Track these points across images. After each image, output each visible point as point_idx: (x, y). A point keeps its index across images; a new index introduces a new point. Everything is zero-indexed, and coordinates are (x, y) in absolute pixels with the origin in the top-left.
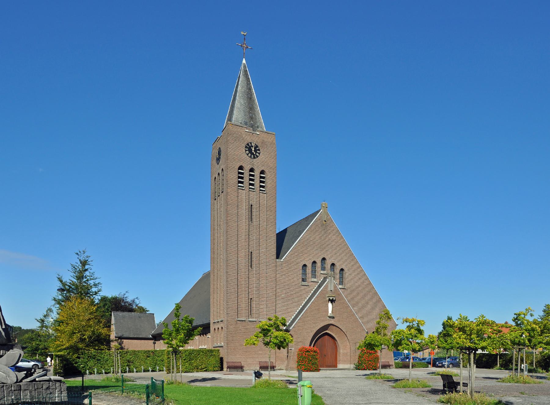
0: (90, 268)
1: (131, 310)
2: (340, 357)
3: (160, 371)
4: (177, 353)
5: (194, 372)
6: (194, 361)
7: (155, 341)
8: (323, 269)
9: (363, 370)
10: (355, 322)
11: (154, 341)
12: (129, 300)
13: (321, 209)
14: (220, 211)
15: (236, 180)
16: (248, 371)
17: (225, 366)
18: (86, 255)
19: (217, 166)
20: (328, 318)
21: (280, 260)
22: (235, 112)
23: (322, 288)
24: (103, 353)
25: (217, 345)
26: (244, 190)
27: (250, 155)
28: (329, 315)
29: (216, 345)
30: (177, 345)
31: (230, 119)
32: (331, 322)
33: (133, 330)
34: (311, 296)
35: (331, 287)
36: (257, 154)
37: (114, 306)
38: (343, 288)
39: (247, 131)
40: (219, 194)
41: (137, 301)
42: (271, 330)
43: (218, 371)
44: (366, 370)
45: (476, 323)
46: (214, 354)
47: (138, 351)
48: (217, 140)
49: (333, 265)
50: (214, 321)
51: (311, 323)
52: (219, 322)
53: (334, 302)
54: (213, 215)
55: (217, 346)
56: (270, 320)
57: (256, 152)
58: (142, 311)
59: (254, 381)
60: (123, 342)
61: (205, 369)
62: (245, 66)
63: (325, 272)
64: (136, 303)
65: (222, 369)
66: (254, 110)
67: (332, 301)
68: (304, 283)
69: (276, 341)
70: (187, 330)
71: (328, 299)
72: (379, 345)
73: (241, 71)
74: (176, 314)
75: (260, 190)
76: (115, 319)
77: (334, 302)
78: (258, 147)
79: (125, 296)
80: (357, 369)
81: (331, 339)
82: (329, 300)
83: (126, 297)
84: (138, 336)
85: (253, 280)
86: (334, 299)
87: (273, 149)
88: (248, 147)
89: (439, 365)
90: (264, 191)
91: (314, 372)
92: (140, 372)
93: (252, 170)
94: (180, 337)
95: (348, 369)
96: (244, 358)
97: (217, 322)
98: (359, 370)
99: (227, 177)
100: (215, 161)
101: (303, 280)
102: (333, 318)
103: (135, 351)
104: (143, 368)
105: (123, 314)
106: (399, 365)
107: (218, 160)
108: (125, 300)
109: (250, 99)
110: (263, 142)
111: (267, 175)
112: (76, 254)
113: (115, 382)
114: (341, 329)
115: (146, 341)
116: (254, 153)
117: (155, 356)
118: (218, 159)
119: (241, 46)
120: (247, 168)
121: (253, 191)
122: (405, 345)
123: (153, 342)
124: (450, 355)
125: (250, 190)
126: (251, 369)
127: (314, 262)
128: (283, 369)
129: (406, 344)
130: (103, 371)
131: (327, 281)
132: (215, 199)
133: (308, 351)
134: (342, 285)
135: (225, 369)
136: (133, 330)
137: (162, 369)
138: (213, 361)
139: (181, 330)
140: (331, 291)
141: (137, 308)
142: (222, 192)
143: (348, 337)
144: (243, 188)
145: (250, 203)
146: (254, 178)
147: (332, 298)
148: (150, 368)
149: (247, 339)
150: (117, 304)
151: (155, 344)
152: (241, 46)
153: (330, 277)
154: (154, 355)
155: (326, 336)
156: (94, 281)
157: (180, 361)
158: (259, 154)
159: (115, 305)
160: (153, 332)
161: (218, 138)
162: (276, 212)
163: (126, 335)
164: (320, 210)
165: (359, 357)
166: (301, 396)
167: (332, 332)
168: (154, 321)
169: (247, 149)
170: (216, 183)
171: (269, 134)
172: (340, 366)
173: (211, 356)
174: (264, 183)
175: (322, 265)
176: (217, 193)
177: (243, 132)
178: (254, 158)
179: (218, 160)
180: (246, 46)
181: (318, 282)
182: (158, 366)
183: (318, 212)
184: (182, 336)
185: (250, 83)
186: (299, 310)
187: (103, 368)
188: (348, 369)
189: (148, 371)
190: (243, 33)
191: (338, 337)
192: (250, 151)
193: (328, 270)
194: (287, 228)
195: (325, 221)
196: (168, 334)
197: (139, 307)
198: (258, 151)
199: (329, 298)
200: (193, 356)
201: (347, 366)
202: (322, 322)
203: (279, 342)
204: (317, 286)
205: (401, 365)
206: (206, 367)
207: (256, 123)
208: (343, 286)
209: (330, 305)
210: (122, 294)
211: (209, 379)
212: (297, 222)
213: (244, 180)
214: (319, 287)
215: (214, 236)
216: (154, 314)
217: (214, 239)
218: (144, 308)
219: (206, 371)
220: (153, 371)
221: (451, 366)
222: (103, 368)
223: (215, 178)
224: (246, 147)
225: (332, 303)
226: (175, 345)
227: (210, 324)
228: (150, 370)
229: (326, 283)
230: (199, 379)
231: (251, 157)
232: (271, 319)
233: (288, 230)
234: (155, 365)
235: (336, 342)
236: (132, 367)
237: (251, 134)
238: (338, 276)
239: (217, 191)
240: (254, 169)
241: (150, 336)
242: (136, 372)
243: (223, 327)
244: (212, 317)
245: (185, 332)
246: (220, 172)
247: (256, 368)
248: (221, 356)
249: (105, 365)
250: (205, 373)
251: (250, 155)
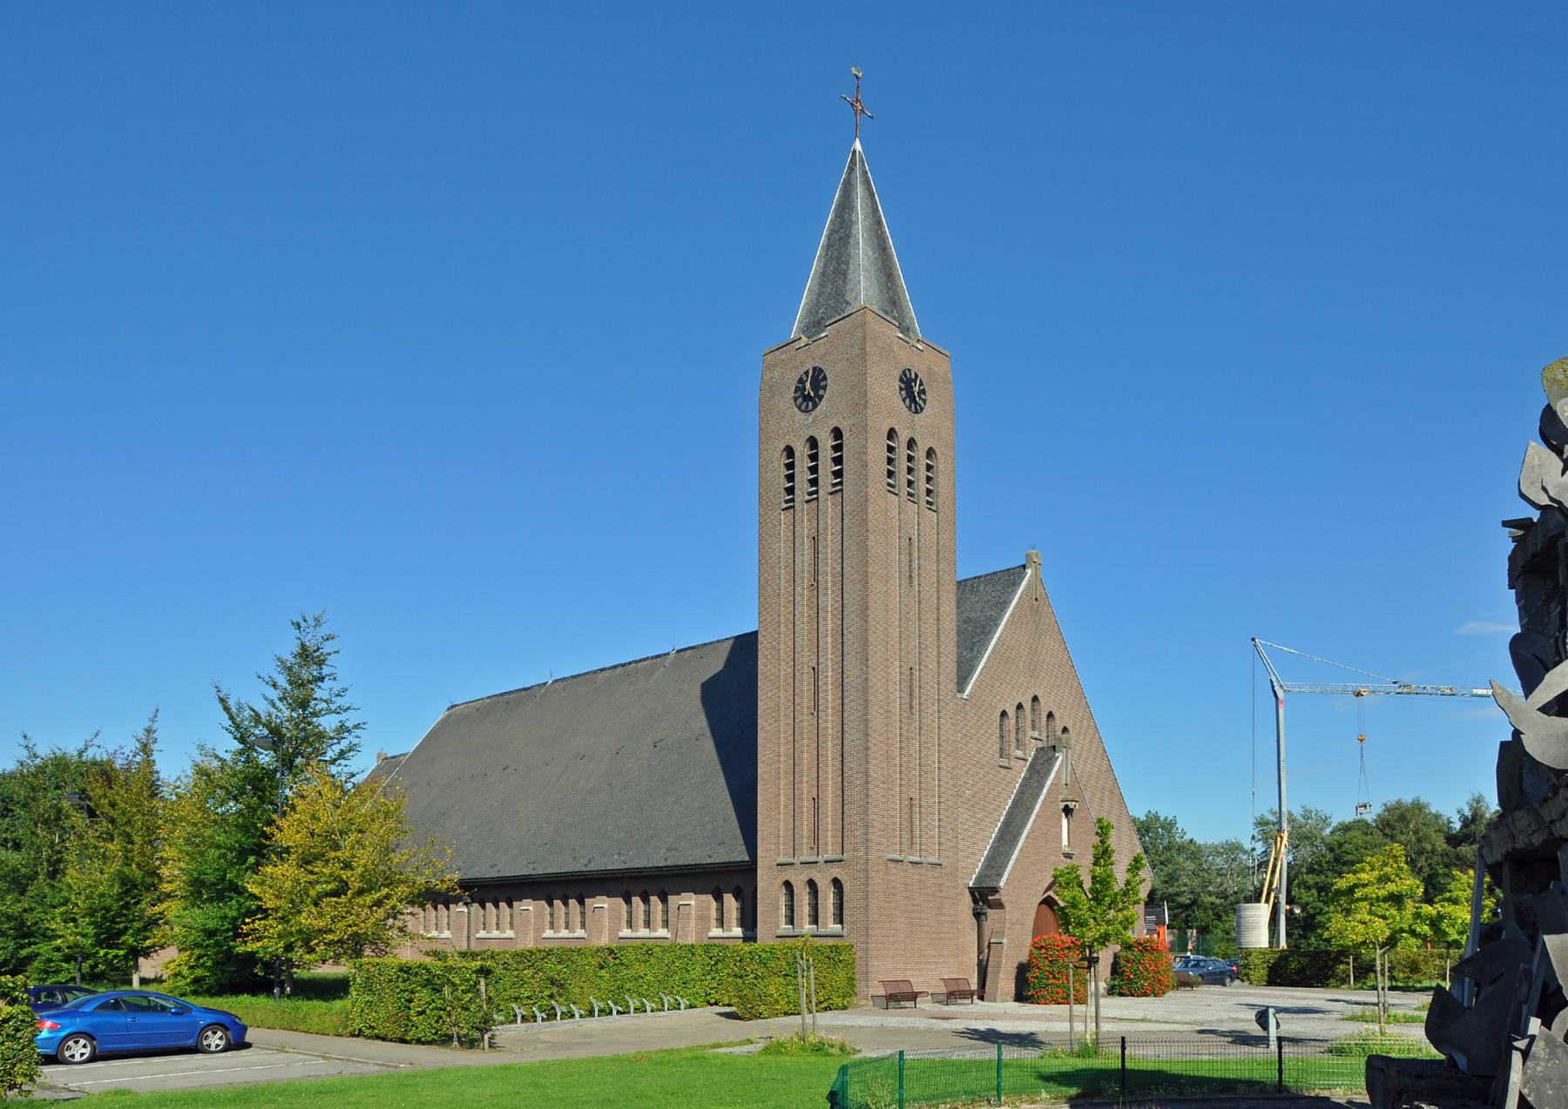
0: (332, 674)
18: (322, 631)
39: (900, 335)
45: (1059, 873)
61: (825, 1005)
71: (1062, 805)
111: (941, 463)
112: (293, 624)
119: (852, 105)
153: (1064, 750)
156: (340, 717)
171: (941, 355)
178: (916, 412)
190: (854, 72)
199: (1065, 803)
213: (895, 468)
231: (909, 408)
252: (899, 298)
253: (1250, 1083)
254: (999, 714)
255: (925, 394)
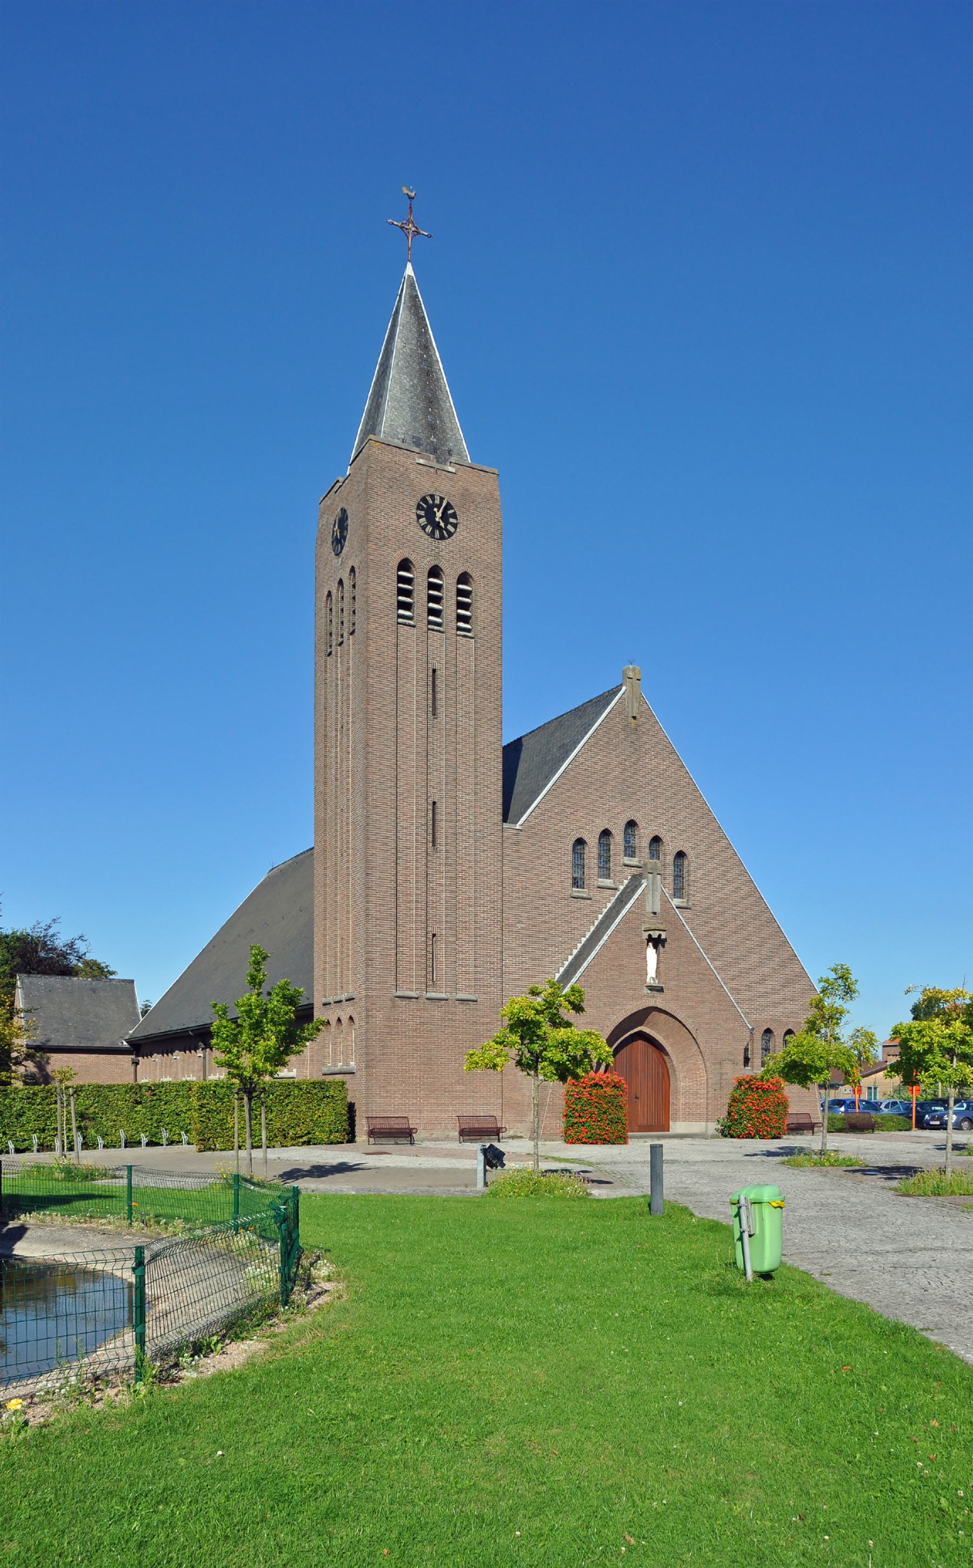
1: (68, 971)
2: (679, 1101)
3: (171, 1143)
4: (255, 1094)
5: (274, 1147)
6: (274, 1114)
7: (137, 1055)
8: (630, 851)
9: (743, 1138)
10: (720, 1003)
11: (133, 1057)
12: (60, 943)
13: (621, 685)
14: (345, 685)
15: (393, 599)
16: (425, 1144)
17: (362, 1127)
19: (337, 561)
20: (646, 991)
21: (512, 826)
22: (388, 405)
23: (628, 906)
24: (11, 1094)
25: (336, 1069)
26: (414, 626)
27: (429, 529)
28: (649, 981)
29: (329, 1066)
30: (255, 1070)
31: (372, 426)
32: (651, 1003)
33: (75, 1027)
34: (598, 928)
35: (653, 902)
36: (450, 528)
37: (18, 960)
38: (684, 905)
39: (422, 461)
40: (340, 640)
41: (81, 946)
42: (540, 1023)
43: (343, 1143)
44: (752, 1138)
46: (332, 1093)
47: (110, 1088)
48: (335, 489)
49: (656, 840)
50: (324, 1000)
51: (601, 1004)
52: (341, 1001)
53: (663, 947)
54: (322, 698)
55: (334, 1072)
56: (534, 993)
57: (447, 523)
58: (96, 973)
59: (480, 1175)
60: (48, 1058)
61: (305, 1139)
62: (412, 286)
63: (634, 861)
64: (78, 952)
65: (351, 1137)
66: (440, 405)
67: (657, 943)
68: (576, 891)
69: (558, 1056)
70: (283, 1024)
71: (645, 935)
72: (822, 1069)
73: (401, 296)
74: (253, 978)
75: (459, 629)
76: (26, 996)
77: (663, 947)
78: (453, 508)
79: (51, 932)
80: (726, 1136)
81: (654, 1048)
82: (650, 939)
83: (52, 936)
84: (89, 1044)
85: (440, 880)
86: (663, 937)
87: (492, 513)
88: (425, 506)
89: (931, 1123)
90: (468, 630)
91: (614, 1143)
92: (114, 1147)
93: (435, 571)
94: (267, 1046)
95: (703, 1136)
96: (413, 1104)
97: (335, 1002)
98: (732, 1137)
99: (366, 589)
100: (328, 546)
101: (577, 883)
102: (660, 990)
103: (100, 1087)
104: (122, 1134)
105: (47, 981)
106: (834, 1123)
107: (337, 544)
108: (48, 943)
109: (428, 375)
110: (466, 495)
111: (475, 587)
113: (63, 1180)
114: (680, 1022)
115: (112, 1058)
116: (442, 524)
117: (157, 1099)
118: (339, 542)
119: (402, 228)
120: (422, 566)
121: (440, 631)
122: (937, 1069)
123: (133, 1059)
124: (935, 1095)
125: (430, 626)
126: (434, 1136)
127: (606, 833)
128: (521, 1137)
129: (939, 1066)
130: (11, 1146)
131: (643, 886)
132: (330, 654)
133: (596, 1085)
134: (680, 898)
135: (361, 1137)
136: (75, 1027)
137: (176, 1138)
138: (329, 1114)
139: (267, 1024)
140: (655, 913)
141: (80, 964)
142: (352, 633)
143: (701, 1044)
144: (411, 622)
145: (430, 666)
146: (440, 594)
147: (658, 933)
148: (142, 1135)
149: (471, 1052)
150: (28, 955)
151: (138, 1066)
152: (402, 228)
153: (650, 875)
154: (155, 1098)
155: (640, 1042)
157: (236, 1115)
158: (455, 526)
159: (23, 956)
160: (131, 1032)
161: (338, 481)
162: (501, 689)
163: (57, 1040)
164: (618, 688)
165: (734, 1100)
166: (750, 1236)
167: (658, 1031)
168: (133, 1000)
169: (422, 513)
170: (331, 610)
172: (677, 1127)
173: (322, 1100)
174: (467, 609)
175: (626, 841)
176: (334, 636)
177: (411, 466)
178: (442, 538)
179: (337, 544)
180: (413, 229)
181: (616, 889)
182: (166, 1129)
183: (614, 692)
184: (273, 1041)
185: (427, 331)
186: (565, 966)
187: (8, 1137)
188: (703, 1136)
189: (139, 1143)
191: (671, 1045)
192: (430, 516)
193: (643, 856)
194: (520, 740)
195: (634, 718)
196: (227, 1036)
197: (87, 963)
198: (452, 520)
200: (271, 1100)
201: (696, 1127)
202: (631, 1003)
203: (568, 1060)
204: (613, 901)
205: (839, 1125)
206: (309, 1133)
207: (443, 441)
208: (683, 902)
209: (651, 953)
210: (43, 925)
211: (333, 1166)
212: (549, 722)
214: (621, 902)
215: (326, 756)
216: (132, 982)
217: (325, 766)
218: (103, 965)
219: (308, 1143)
220: (150, 1144)
221: (965, 1124)
222: (8, 1137)
223: (329, 594)
224: (419, 507)
225: (655, 947)
226: (250, 1069)
227: (313, 1008)
228: (145, 1141)
229: (640, 891)
230: (306, 1168)
231: (432, 535)
232: (539, 990)
233: (524, 741)
234: (158, 1127)
235: (666, 1058)
236: (92, 1132)
237: (432, 470)
238: (670, 870)
239: (334, 631)
240: (442, 570)
241: (125, 1043)
242: (104, 1146)
243: (355, 1016)
244: (317, 987)
245: (280, 1031)
246: (346, 577)
247: (447, 1133)
248: (349, 1100)
249: (14, 1129)
250: (305, 1149)
251: (429, 529)
252: (442, 421)
253: (438, 1157)
254: (572, 842)
255: (456, 518)
